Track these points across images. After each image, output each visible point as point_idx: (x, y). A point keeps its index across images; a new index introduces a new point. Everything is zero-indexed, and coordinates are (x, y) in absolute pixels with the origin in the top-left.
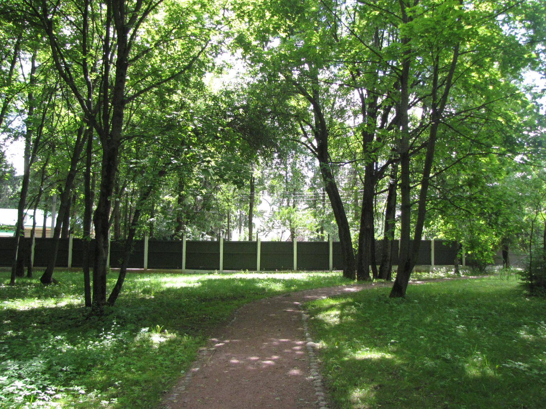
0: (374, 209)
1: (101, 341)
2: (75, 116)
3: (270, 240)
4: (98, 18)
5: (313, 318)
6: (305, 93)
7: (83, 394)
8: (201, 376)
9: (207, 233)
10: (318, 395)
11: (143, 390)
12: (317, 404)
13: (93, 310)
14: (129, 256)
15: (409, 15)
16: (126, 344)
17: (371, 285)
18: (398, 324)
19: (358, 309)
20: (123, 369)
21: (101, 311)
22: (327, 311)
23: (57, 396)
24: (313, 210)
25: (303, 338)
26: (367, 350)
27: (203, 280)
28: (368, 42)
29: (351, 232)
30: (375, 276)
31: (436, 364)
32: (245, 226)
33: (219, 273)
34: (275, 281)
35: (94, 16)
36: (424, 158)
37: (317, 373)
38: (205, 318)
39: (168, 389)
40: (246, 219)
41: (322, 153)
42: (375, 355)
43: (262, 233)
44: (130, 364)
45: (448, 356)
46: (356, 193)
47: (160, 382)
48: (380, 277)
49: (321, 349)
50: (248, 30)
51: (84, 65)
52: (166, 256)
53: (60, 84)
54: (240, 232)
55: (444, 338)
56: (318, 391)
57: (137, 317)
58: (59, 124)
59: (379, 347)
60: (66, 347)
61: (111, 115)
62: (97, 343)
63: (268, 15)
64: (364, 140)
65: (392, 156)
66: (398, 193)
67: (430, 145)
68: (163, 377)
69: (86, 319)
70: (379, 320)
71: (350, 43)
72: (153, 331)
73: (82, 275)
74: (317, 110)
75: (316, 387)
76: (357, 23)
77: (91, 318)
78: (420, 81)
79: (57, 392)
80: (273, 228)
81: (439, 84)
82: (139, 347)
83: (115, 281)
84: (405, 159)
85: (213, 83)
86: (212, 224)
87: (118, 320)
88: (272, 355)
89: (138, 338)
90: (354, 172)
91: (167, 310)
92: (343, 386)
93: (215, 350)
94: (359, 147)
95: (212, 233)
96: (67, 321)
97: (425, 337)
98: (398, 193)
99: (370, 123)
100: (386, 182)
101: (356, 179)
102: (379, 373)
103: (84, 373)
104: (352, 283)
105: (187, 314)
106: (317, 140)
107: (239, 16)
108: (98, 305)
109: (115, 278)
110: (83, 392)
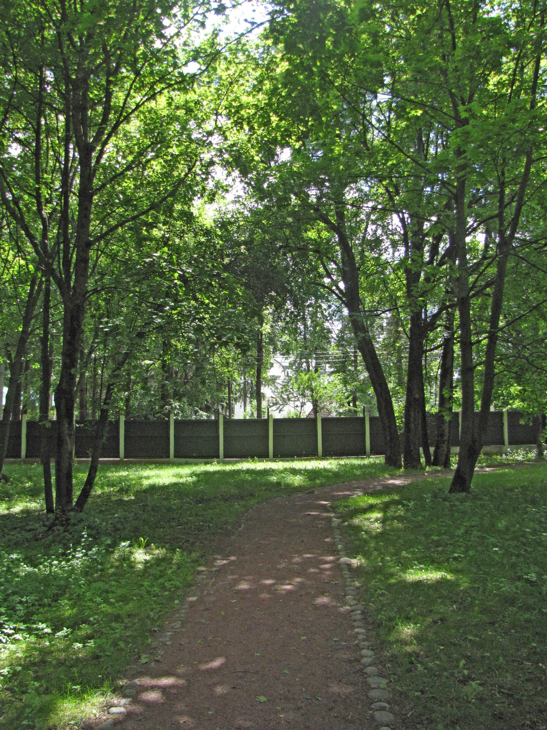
0: (424, 372)
1: (68, 561)
2: (27, 265)
3: (286, 417)
4: (54, 133)
5: (346, 523)
6: (327, 221)
7: (49, 634)
8: (202, 608)
9: (201, 409)
10: (358, 633)
11: (126, 628)
12: (357, 645)
13: (57, 519)
14: (99, 442)
15: (464, 115)
16: (101, 564)
17: (424, 474)
18: (462, 531)
19: (407, 510)
20: (98, 599)
21: (68, 520)
22: (365, 513)
23: (17, 636)
24: (341, 375)
25: (334, 552)
26: (421, 569)
27: (198, 472)
28: (409, 148)
29: (394, 402)
30: (428, 462)
31: (517, 588)
32: (251, 397)
33: (218, 463)
34: (294, 472)
35: (50, 131)
36: (490, 301)
37: (355, 602)
38: (202, 526)
39: (158, 626)
40: (252, 388)
41: (351, 299)
42: (433, 575)
43: (274, 408)
44: (107, 592)
45: (533, 576)
46: (399, 351)
47: (148, 617)
48: (435, 463)
49: (360, 568)
50: (249, 141)
51: (38, 197)
52: (149, 446)
53: (7, 220)
54: (245, 406)
55: (526, 550)
56: (358, 627)
57: (115, 526)
58: (6, 271)
59: (438, 563)
60: (25, 569)
61: (74, 260)
62: (63, 563)
63: (274, 119)
64: (407, 279)
65: (445, 300)
66: (457, 349)
67: (498, 281)
68: (152, 610)
69: (48, 530)
70: (435, 526)
71: (385, 153)
72: (136, 546)
73: (41, 469)
74: (343, 242)
75: (355, 621)
76: (393, 124)
77: (55, 528)
78: (481, 198)
79: (17, 630)
80: (289, 399)
81: (506, 200)
82: (117, 567)
83: (84, 476)
84: (464, 304)
85: (206, 213)
86: (208, 397)
87: (89, 531)
88: (294, 576)
89: (116, 556)
90: (396, 322)
91: (153, 514)
92: (391, 619)
93: (218, 571)
94: (400, 289)
95: (207, 409)
96: (24, 533)
97: (501, 549)
98: (457, 349)
99: (415, 258)
100: (439, 335)
101: (399, 332)
102: (439, 601)
103: (49, 605)
104: (398, 473)
105: (179, 521)
106: (345, 283)
107: (236, 123)
108: (63, 511)
109: (84, 472)
110: (48, 630)
